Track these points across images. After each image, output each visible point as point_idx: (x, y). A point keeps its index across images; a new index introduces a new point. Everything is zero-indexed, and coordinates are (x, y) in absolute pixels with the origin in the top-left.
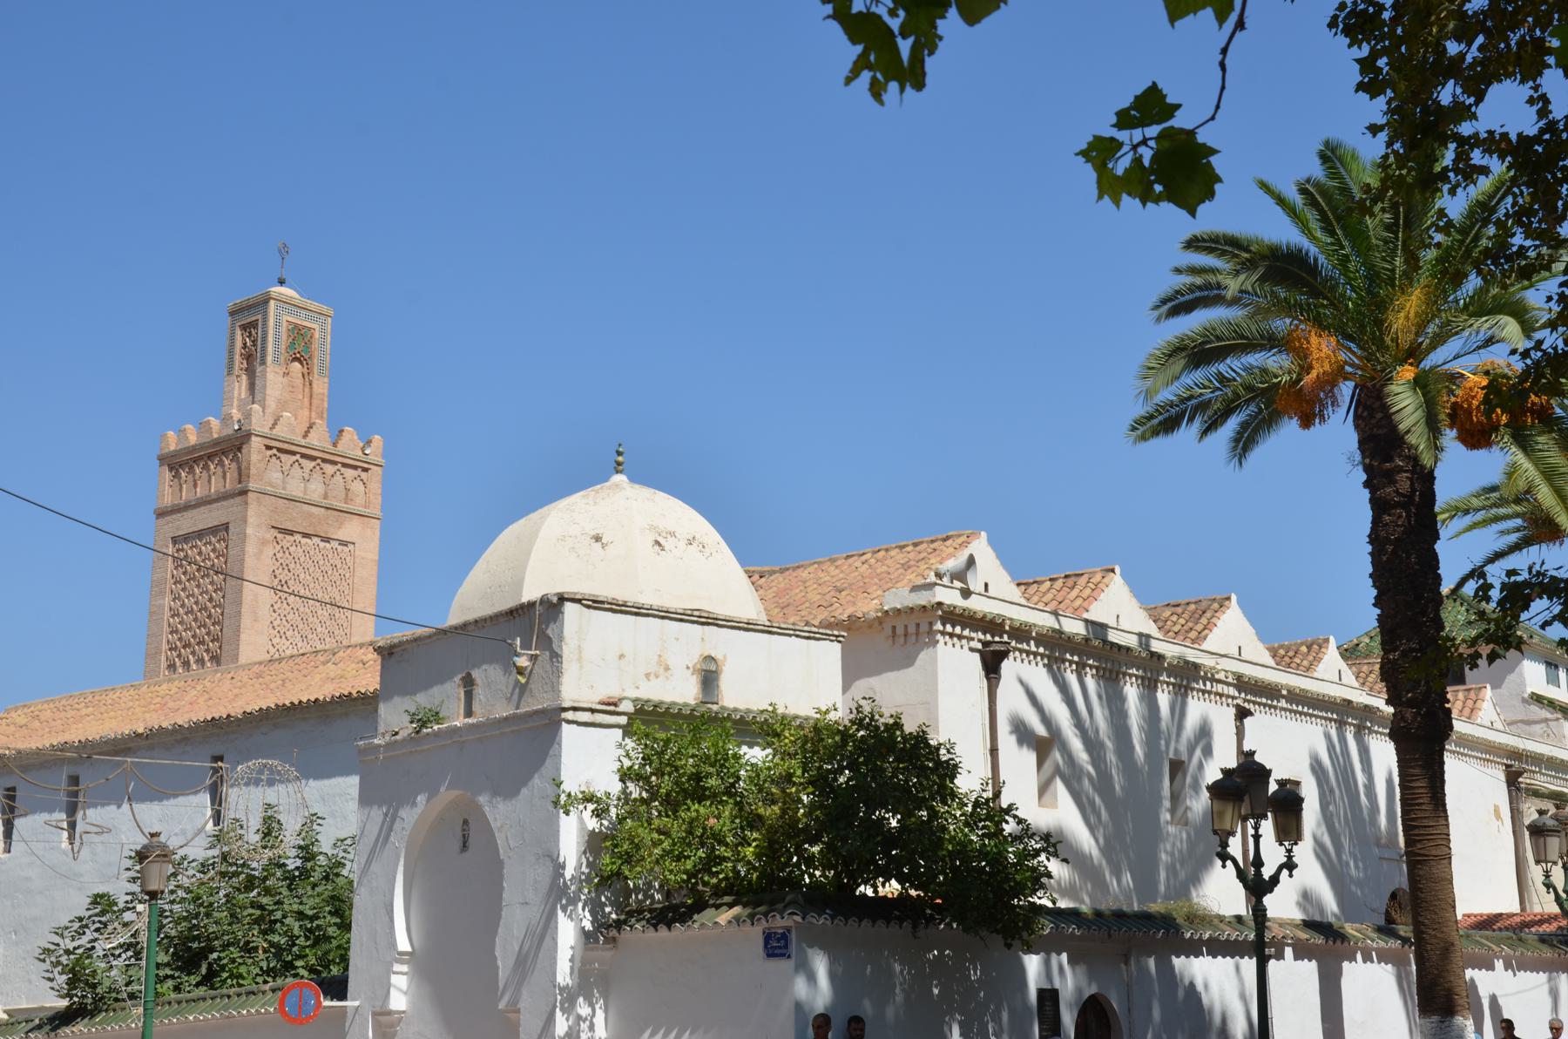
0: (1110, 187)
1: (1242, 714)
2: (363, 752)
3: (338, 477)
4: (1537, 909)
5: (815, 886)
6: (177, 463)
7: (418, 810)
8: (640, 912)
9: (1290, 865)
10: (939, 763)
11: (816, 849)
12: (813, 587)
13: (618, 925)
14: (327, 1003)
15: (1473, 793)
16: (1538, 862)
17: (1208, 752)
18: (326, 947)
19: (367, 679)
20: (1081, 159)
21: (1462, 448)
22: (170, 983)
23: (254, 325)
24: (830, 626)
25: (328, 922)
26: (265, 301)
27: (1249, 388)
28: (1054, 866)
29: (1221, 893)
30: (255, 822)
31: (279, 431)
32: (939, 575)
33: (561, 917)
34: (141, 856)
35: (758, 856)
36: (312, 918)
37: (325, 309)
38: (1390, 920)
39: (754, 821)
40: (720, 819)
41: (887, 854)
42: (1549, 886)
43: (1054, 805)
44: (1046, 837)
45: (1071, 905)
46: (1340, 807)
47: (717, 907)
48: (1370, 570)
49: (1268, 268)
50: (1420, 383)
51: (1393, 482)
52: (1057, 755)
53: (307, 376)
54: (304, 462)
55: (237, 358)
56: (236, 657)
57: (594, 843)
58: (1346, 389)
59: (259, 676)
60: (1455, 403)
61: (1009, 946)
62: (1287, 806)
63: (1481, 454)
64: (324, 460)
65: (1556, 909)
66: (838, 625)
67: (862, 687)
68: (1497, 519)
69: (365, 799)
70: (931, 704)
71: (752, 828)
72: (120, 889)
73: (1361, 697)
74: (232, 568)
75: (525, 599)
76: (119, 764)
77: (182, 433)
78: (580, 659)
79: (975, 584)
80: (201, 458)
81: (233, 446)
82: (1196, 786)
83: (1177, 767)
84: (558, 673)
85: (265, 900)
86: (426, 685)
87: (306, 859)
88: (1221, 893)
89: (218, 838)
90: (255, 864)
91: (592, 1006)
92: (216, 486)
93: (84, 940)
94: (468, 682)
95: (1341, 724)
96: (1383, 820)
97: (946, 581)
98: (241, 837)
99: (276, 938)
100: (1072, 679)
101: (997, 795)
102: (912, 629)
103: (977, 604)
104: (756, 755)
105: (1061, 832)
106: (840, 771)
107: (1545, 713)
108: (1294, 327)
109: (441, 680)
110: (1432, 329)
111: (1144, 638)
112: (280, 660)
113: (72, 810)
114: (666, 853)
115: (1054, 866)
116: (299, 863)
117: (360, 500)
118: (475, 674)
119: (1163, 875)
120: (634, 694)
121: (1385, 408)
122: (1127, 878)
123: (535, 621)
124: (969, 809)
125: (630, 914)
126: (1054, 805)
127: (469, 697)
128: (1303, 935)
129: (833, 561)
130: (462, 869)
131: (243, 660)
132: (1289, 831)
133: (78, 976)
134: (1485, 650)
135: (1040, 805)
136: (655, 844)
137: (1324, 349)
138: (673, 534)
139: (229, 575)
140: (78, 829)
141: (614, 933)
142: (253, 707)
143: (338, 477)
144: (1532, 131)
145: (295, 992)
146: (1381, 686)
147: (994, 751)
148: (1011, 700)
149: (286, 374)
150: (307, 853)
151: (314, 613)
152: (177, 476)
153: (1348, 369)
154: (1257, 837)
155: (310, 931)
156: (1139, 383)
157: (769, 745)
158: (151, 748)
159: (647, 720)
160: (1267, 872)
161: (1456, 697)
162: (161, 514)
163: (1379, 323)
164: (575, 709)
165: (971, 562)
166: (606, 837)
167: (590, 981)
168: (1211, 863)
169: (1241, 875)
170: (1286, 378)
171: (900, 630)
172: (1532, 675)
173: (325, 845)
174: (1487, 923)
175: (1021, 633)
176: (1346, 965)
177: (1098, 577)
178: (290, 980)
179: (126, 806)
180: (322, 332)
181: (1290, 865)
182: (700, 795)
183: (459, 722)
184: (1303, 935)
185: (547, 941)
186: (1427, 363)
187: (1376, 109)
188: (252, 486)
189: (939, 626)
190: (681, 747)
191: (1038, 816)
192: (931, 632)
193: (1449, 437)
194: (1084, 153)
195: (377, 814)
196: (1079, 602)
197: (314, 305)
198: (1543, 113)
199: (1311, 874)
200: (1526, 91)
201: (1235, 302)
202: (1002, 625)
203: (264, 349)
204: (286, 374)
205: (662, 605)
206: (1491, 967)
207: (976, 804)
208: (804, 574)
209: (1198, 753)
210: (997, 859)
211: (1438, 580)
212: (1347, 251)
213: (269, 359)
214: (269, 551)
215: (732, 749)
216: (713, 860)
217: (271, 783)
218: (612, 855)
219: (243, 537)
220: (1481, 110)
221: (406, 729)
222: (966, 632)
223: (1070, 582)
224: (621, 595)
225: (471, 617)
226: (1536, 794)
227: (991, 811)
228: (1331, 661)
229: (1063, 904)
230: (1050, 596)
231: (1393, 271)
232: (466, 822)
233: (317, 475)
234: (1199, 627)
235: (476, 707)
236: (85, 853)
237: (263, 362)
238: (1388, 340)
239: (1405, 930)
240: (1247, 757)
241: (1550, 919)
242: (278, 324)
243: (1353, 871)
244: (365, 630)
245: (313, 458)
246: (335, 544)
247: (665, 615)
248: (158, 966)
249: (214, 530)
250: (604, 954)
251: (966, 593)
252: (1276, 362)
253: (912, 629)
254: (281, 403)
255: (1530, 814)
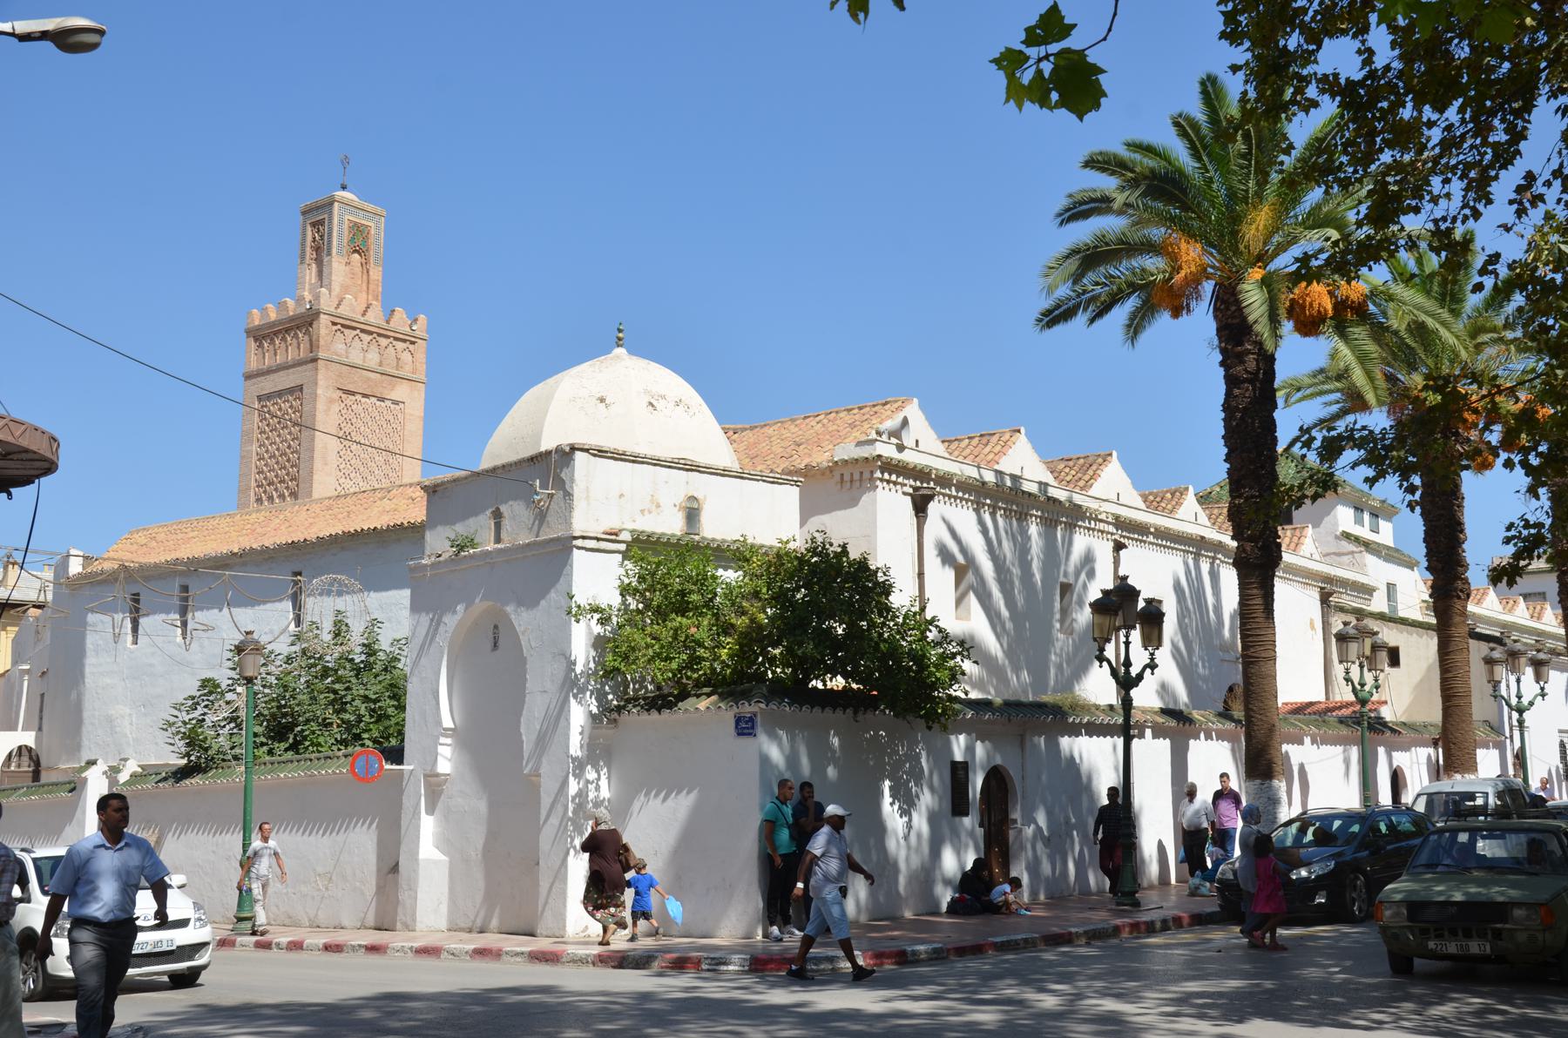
0: (1016, 93)
1: (1119, 547)
2: (412, 570)
3: (391, 349)
4: (1338, 698)
5: (776, 680)
6: (262, 335)
7: (458, 617)
8: (636, 699)
9: (1152, 666)
10: (877, 584)
11: (777, 651)
12: (777, 441)
13: (619, 709)
14: (388, 767)
15: (1295, 611)
16: (1341, 662)
17: (1091, 574)
18: (387, 723)
19: (416, 512)
20: (994, 67)
21: (1297, 336)
22: (265, 748)
23: (321, 222)
24: (790, 473)
25: (388, 704)
26: (330, 203)
27: (1131, 285)
28: (967, 666)
29: (1098, 688)
30: (328, 625)
31: (343, 310)
32: (879, 433)
33: (572, 701)
34: (239, 649)
35: (731, 656)
36: (375, 701)
37: (379, 210)
38: (1227, 708)
39: (727, 629)
40: (699, 628)
41: (834, 656)
42: (1348, 680)
43: (968, 618)
44: (962, 643)
45: (980, 696)
46: (1193, 622)
47: (698, 696)
48: (1223, 432)
49: (1149, 187)
50: (1266, 282)
51: (1243, 362)
52: (970, 577)
53: (365, 265)
54: (363, 336)
55: (308, 249)
56: (310, 494)
57: (599, 643)
58: (1208, 287)
59: (329, 508)
60: (1292, 300)
61: (930, 728)
62: (1152, 618)
63: (1310, 340)
64: (380, 335)
65: (1352, 698)
66: (797, 472)
67: (816, 522)
68: (1321, 393)
69: (416, 607)
70: (871, 536)
71: (726, 634)
72: (223, 676)
73: (1212, 534)
74: (306, 421)
75: (543, 449)
76: (220, 576)
77: (264, 311)
78: (587, 498)
79: (908, 441)
80: (279, 331)
81: (306, 321)
82: (1081, 603)
83: (1066, 589)
84: (570, 508)
85: (337, 686)
86: (464, 517)
87: (369, 655)
88: (1098, 688)
89: (298, 637)
90: (328, 658)
91: (598, 772)
92: (292, 355)
93: (196, 714)
94: (497, 515)
95: (1197, 556)
96: (1227, 633)
97: (885, 438)
98: (317, 636)
99: (346, 716)
100: (987, 517)
101: (923, 609)
102: (856, 476)
103: (909, 457)
104: (730, 576)
105: (972, 638)
106: (798, 589)
107: (1352, 547)
108: (1163, 235)
109: (475, 513)
110: (1276, 239)
111: (1043, 486)
112: (346, 496)
113: (183, 612)
114: (658, 655)
115: (967, 666)
116: (363, 657)
117: (408, 368)
118: (503, 508)
119: (1052, 671)
120: (631, 526)
121: (1238, 302)
122: (1025, 675)
123: (549, 468)
124: (900, 620)
125: (628, 701)
126: (968, 618)
127: (498, 527)
128: (1160, 720)
129: (793, 420)
130: (493, 661)
131: (316, 495)
132: (1153, 638)
133: (193, 740)
134: (1310, 492)
135: (956, 615)
136: (648, 646)
137: (1192, 254)
138: (663, 397)
139: (304, 426)
140: (190, 627)
141: (615, 715)
142: (325, 533)
143: (391, 349)
144: (1358, 76)
145: (363, 758)
146: (1228, 525)
147: (921, 575)
148: (935, 529)
149: (348, 264)
150: (370, 649)
151: (372, 459)
152: (261, 346)
153: (1210, 270)
154: (1127, 644)
155: (373, 710)
156: (1042, 280)
157: (741, 568)
158: (244, 564)
159: (642, 547)
160: (1134, 671)
161: (1285, 535)
162: (248, 377)
163: (1234, 234)
164: (584, 538)
165: (905, 422)
166: (609, 640)
167: (597, 752)
168: (1092, 663)
169: (1114, 673)
170: (1160, 277)
171: (847, 478)
172: (1344, 517)
173: (384, 644)
174: (1300, 709)
175: (944, 480)
176: (1192, 742)
177: (1007, 436)
178: (358, 748)
179: (226, 610)
180: (377, 229)
181: (1152, 666)
182: (682, 608)
183: (490, 547)
184: (1160, 720)
185: (562, 722)
186: (1272, 267)
187: (1241, 54)
188: (321, 355)
189: (878, 474)
190: (669, 573)
191: (952, 623)
192: (872, 479)
193: (1287, 326)
194: (996, 61)
195: (425, 619)
196: (991, 456)
197: (370, 207)
198: (1368, 62)
199: (1168, 670)
200: (1357, 44)
201: (1120, 213)
202: (929, 473)
203: (330, 242)
204: (348, 264)
205: (654, 454)
206: (1301, 743)
207: (906, 617)
208: (769, 431)
209: (1083, 576)
210: (920, 659)
211: (1275, 441)
212: (1212, 173)
213: (334, 251)
214: (336, 407)
215: (710, 570)
216: (694, 660)
217: (340, 594)
218: (614, 655)
219: (315, 397)
220: (1320, 56)
221: (449, 551)
222: (900, 480)
223: (984, 440)
224: (621, 446)
225: (499, 462)
226: (1342, 610)
227: (920, 621)
228: (1190, 505)
229: (974, 695)
230: (968, 451)
231: (1247, 191)
232: (496, 627)
233: (374, 347)
234: (1087, 477)
235: (504, 535)
236: (195, 646)
237: (329, 254)
238: (1241, 247)
239: (1239, 713)
240: (1122, 580)
241: (1348, 705)
242: (341, 222)
243: (1201, 670)
244: (413, 472)
245: (370, 333)
246: (388, 403)
247: (657, 462)
248: (256, 735)
249: (291, 391)
250: (606, 731)
251: (901, 448)
252: (1153, 264)
253: (856, 476)
254: (344, 288)
255: (1337, 625)
